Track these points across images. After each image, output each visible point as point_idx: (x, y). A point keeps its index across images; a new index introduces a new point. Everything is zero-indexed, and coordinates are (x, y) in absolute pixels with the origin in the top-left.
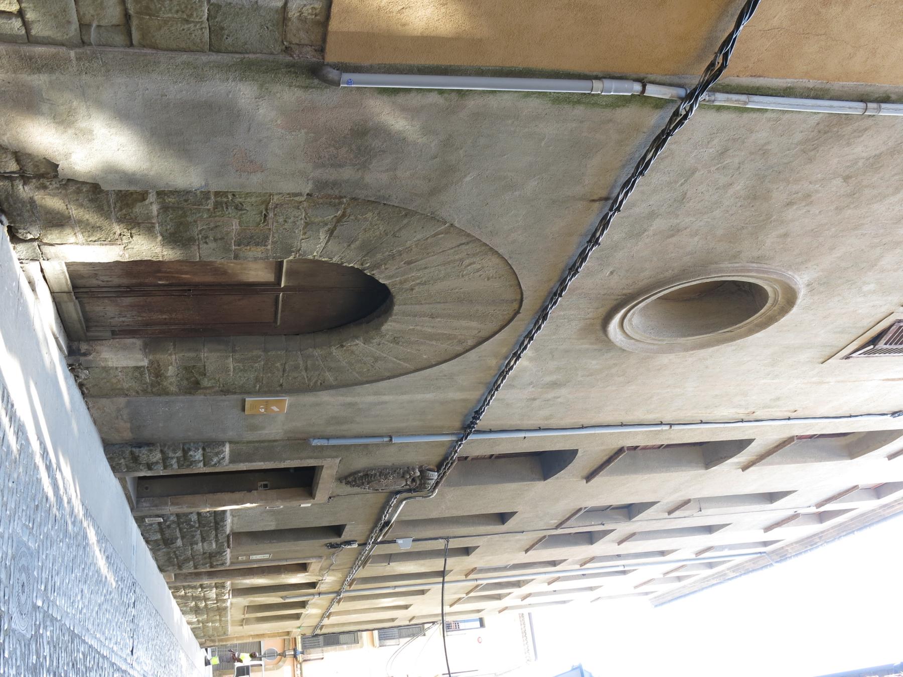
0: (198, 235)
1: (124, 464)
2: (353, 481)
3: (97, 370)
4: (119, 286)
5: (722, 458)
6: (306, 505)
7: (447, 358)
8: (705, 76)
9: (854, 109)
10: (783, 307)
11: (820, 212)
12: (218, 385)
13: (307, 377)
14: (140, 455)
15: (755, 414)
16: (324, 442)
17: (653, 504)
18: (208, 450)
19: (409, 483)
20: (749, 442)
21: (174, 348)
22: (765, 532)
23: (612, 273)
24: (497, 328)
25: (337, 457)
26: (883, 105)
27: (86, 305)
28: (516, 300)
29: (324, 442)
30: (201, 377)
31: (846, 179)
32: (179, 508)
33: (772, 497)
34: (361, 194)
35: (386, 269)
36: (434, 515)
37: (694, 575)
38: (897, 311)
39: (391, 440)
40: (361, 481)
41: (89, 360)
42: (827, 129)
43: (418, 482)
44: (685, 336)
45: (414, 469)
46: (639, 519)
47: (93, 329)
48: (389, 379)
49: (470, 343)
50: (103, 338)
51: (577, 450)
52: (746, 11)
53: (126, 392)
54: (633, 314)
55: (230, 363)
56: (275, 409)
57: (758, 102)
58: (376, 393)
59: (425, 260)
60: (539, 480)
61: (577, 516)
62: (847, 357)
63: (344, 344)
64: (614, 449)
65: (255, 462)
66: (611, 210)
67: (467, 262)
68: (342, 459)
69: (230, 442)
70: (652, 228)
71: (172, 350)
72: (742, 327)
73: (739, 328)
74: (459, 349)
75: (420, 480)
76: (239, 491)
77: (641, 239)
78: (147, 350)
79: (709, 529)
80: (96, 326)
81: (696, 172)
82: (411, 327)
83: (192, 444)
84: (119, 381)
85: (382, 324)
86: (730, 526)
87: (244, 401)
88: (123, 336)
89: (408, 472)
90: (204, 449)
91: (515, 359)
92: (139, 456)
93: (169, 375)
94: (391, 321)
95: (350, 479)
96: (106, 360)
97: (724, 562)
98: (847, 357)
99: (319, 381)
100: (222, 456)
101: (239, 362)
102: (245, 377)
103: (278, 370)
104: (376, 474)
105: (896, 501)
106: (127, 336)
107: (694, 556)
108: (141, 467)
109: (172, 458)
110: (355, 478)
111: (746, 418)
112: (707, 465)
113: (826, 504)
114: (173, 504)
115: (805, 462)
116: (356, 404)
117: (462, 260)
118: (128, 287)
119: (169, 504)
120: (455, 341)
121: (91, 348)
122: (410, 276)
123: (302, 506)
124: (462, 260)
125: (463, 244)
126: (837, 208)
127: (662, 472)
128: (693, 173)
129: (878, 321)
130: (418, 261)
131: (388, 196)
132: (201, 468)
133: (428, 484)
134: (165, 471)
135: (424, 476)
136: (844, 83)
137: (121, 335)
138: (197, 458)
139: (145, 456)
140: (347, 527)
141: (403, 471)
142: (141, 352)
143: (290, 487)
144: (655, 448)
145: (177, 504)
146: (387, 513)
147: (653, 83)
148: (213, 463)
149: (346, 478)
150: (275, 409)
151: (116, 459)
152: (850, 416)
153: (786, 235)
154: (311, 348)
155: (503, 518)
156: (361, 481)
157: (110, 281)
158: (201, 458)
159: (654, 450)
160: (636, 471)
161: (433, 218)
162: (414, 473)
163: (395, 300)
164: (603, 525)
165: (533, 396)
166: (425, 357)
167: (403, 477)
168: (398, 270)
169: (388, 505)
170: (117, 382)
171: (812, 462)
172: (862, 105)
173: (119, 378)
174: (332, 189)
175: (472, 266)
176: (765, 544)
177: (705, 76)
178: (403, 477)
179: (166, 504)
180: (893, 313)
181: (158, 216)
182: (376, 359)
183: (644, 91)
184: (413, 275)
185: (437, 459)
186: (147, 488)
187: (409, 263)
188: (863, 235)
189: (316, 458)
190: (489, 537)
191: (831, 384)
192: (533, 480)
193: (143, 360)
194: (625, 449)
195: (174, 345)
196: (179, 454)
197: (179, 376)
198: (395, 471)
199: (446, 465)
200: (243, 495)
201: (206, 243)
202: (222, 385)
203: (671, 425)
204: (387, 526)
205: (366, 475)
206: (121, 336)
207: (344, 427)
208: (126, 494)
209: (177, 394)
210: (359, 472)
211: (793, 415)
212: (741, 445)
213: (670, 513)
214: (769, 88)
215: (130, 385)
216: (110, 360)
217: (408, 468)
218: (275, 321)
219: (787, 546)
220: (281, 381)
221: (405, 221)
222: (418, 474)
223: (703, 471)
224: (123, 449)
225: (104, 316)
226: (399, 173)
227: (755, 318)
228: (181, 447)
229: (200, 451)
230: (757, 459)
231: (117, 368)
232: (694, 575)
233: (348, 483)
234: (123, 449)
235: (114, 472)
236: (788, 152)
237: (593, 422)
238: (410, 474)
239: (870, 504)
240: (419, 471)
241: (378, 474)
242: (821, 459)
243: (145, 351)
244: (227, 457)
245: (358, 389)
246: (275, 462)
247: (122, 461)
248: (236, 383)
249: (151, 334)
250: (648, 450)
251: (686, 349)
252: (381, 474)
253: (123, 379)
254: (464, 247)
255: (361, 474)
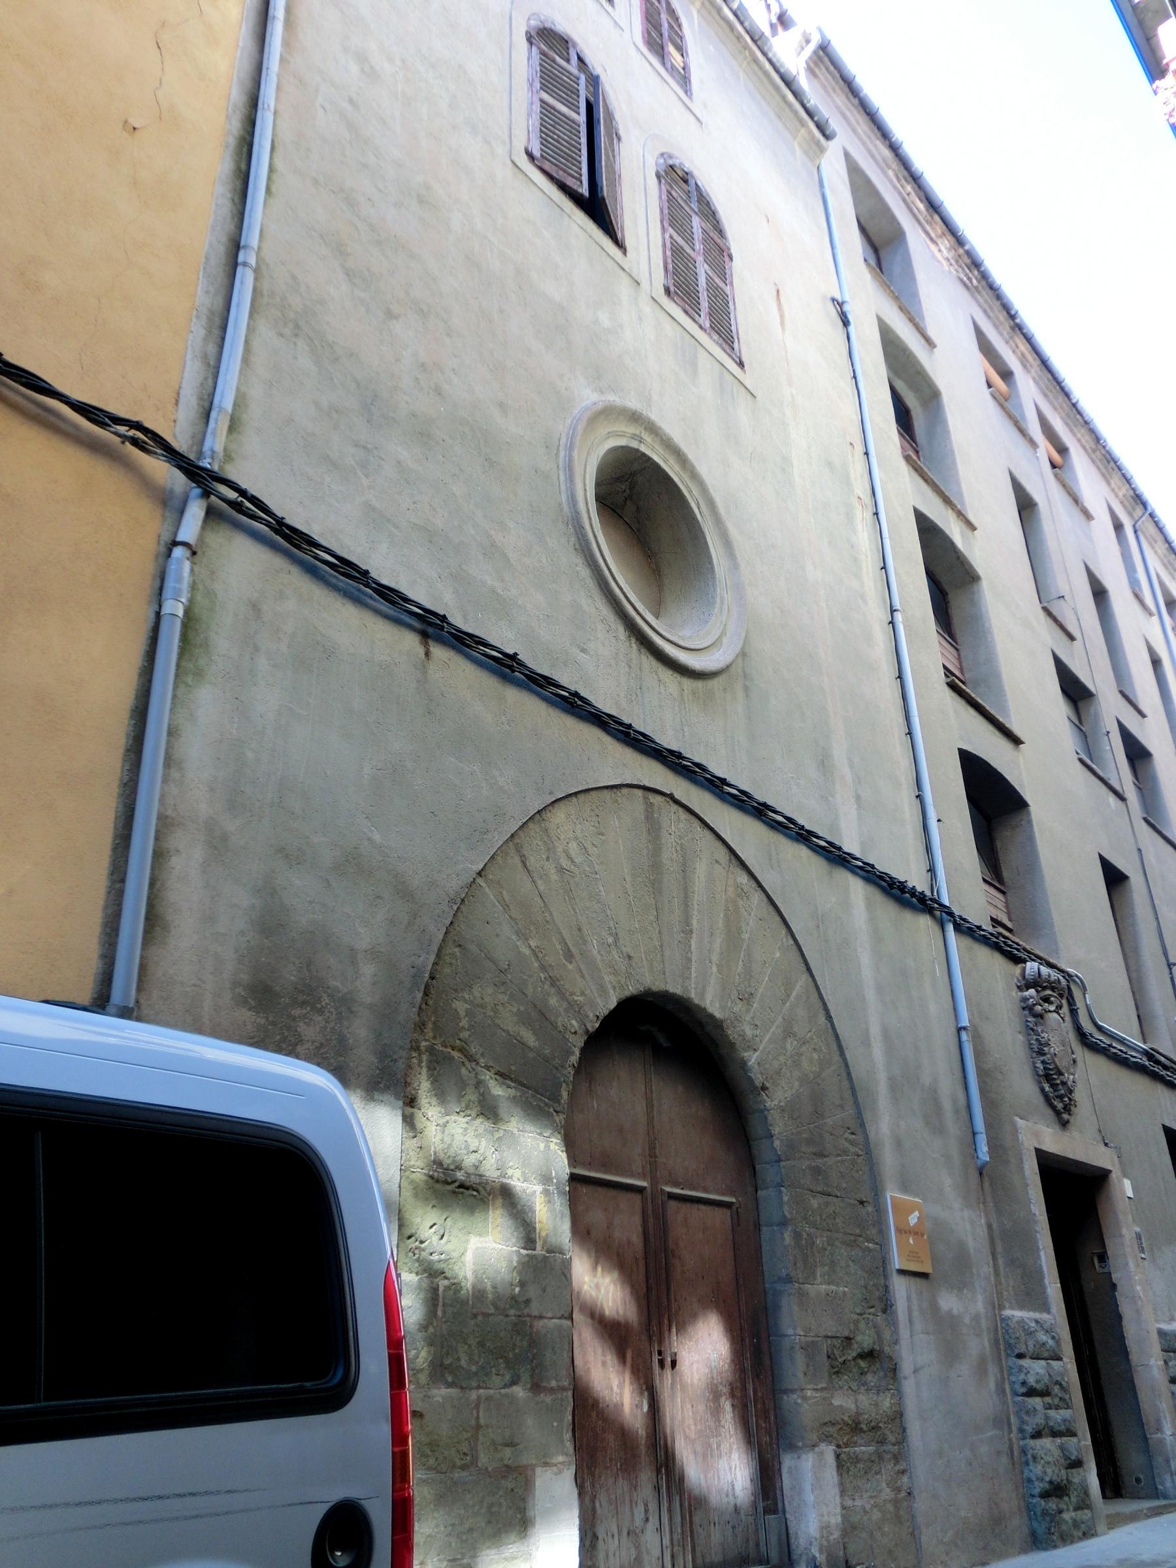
0: (507, 1316)
1: (1073, 1514)
2: (1062, 1101)
3: (852, 1548)
4: (657, 1489)
5: (958, 558)
6: (1125, 1187)
7: (778, 919)
8: (155, 453)
9: (246, 281)
10: (645, 429)
11: (455, 356)
12: (871, 1317)
13: (839, 1155)
14: (1048, 1479)
15: (861, 496)
16: (982, 1140)
17: (1058, 662)
18: (1022, 1349)
19: (1052, 1008)
20: (921, 518)
21: (792, 1391)
22: (1093, 519)
23: (583, 651)
24: (708, 833)
25: (1014, 1124)
26: (242, 243)
27: (707, 1560)
28: (646, 798)
29: (982, 1140)
30: (855, 1346)
31: (390, 315)
32: (1165, 1418)
33: (1026, 506)
34: (408, 1013)
35: (583, 994)
36: (1121, 980)
37: (1158, 576)
38: (649, 292)
39: (964, 1028)
40: (1060, 1087)
41: (828, 1561)
42: (291, 325)
43: (1048, 992)
44: (712, 568)
45: (1025, 1000)
46: (1092, 683)
47: (763, 1549)
48: (831, 1017)
49: (743, 879)
50: (784, 1537)
51: (959, 749)
52: (24, 380)
53: (903, 1494)
54: (683, 638)
55: (819, 1288)
56: (913, 1219)
57: (226, 399)
58: (866, 1042)
59: (561, 929)
60: (1029, 814)
61: (1094, 766)
62: (741, 364)
63: (758, 1084)
64: (951, 697)
65: (1041, 1266)
66: (442, 628)
67: (565, 863)
68: (1017, 1115)
69: (1001, 1307)
70: (489, 582)
71: (795, 1396)
72: (687, 487)
73: (690, 492)
74: (757, 897)
75: (1044, 988)
76: (1118, 1306)
77: (510, 600)
78: (800, 1444)
79: (1100, 594)
80: (757, 1545)
81: (370, 505)
82: (714, 969)
83: (1013, 1378)
84: (875, 1506)
85: (712, 1017)
86: (1088, 563)
87: (901, 1272)
88: (778, 1493)
89: (1030, 1009)
90: (1020, 1356)
91: (771, 814)
92: (1051, 1482)
93: (853, 1407)
94: (702, 995)
95: (1060, 1106)
96: (825, 1528)
97: (1162, 584)
98: (741, 364)
99: (847, 1135)
100: (1033, 1324)
101: (814, 1273)
102: (848, 1266)
103: (827, 1204)
104: (1043, 1062)
105: (1014, 352)
106: (778, 1485)
107: (1155, 619)
108: (1076, 1480)
109: (1047, 1418)
110: (1057, 1097)
111: (871, 510)
112: (974, 578)
113: (1029, 435)
114: (1159, 1429)
115: (953, 452)
116: (892, 1080)
117: (561, 870)
118: (658, 1471)
119: (1159, 1435)
120: (740, 903)
121: (804, 1557)
122: (599, 957)
123: (1130, 1193)
124: (561, 870)
125: (524, 863)
126: (448, 335)
127: (992, 638)
128: (374, 509)
129: (669, 318)
130: (564, 939)
131: (413, 970)
132: (1068, 1367)
133: (1049, 976)
134: (1080, 1434)
135: (1036, 983)
136: (199, 289)
137: (775, 1494)
138: (1042, 1371)
139: (1049, 1471)
140: (1168, 1124)
141: (1033, 1015)
142: (804, 1456)
143: (1097, 1212)
144: (959, 655)
145: (1158, 1421)
146: (1126, 1053)
147: (175, 534)
148: (1051, 1342)
149: (1058, 1113)
150: (913, 1219)
151: (1064, 1527)
152: (855, 377)
153: (502, 406)
154: (773, 1143)
155: (1114, 878)
156: (1060, 1087)
157: (646, 1505)
158: (1043, 1362)
159: (962, 656)
160: (997, 676)
161: (463, 901)
162: (1032, 997)
163: (655, 988)
164: (1108, 732)
165: (853, 800)
166: (778, 955)
167: (1041, 1016)
168: (587, 976)
169: (1109, 1050)
170: (880, 1510)
171: (951, 443)
172: (240, 269)
173: (868, 1507)
174: (395, 1061)
175: (573, 854)
176: (1118, 527)
177: (155, 453)
178: (1041, 1016)
179: (1162, 1442)
180: (653, 298)
181: (462, 1388)
182: (788, 1032)
183: (185, 544)
184: (596, 952)
185: (998, 962)
186: (1138, 1480)
187: (569, 956)
188: (501, 311)
189: (1021, 1159)
190: (1156, 902)
191: (794, 392)
192: (1030, 822)
193: (822, 1453)
194: (949, 680)
195: (787, 1391)
196: (1036, 1402)
197: (855, 1388)
198: (1033, 1030)
199: (1010, 946)
200: (1122, 1299)
201: (528, 1301)
202: (872, 1310)
203: (893, 611)
204: (1153, 1056)
205: (1048, 1077)
206: (779, 1496)
207: (947, 1105)
208: (1148, 1517)
209: (899, 1394)
210: (1042, 1090)
211: (860, 449)
212: (928, 531)
213: (1072, 638)
214: (202, 384)
215: (884, 1485)
216: (826, 1518)
217: (1024, 1009)
218: (728, 1205)
219: (1117, 496)
220: (852, 1202)
221: (473, 948)
222: (1032, 991)
223: (985, 584)
224: (1039, 1513)
225: (733, 1527)
226: (362, 944)
227: (657, 455)
228: (1020, 1398)
229: (1026, 1363)
230: (952, 509)
231: (844, 1508)
232: (1158, 576)
233: (1067, 1109)
234: (1039, 1513)
235: (1094, 1535)
236: (335, 380)
237: (901, 719)
238: (1034, 1005)
239: (1028, 388)
240: (1027, 989)
241: (1042, 1058)
242: (946, 432)
243: (801, 1448)
244: (1037, 1315)
245: (858, 1070)
246: (1036, 1231)
247: (1066, 1516)
248: (862, 1282)
249: (771, 1437)
250: (963, 664)
251: (735, 566)
252: (1041, 1053)
253: (871, 1497)
254: (532, 861)
255: (1047, 1088)
